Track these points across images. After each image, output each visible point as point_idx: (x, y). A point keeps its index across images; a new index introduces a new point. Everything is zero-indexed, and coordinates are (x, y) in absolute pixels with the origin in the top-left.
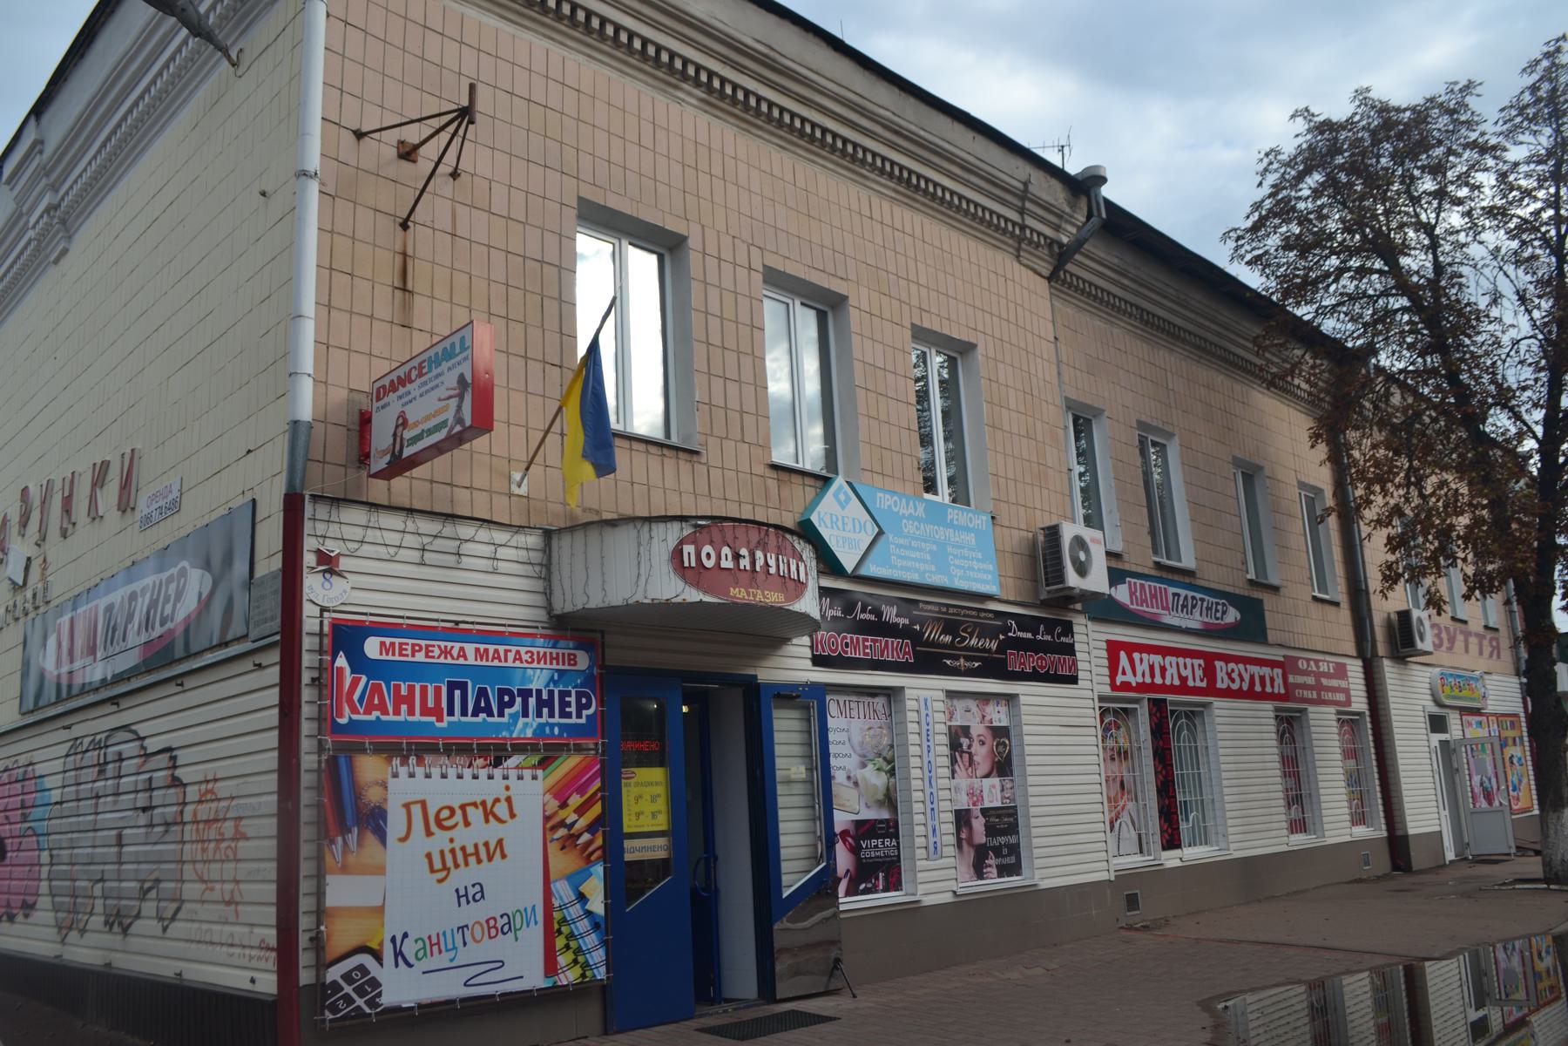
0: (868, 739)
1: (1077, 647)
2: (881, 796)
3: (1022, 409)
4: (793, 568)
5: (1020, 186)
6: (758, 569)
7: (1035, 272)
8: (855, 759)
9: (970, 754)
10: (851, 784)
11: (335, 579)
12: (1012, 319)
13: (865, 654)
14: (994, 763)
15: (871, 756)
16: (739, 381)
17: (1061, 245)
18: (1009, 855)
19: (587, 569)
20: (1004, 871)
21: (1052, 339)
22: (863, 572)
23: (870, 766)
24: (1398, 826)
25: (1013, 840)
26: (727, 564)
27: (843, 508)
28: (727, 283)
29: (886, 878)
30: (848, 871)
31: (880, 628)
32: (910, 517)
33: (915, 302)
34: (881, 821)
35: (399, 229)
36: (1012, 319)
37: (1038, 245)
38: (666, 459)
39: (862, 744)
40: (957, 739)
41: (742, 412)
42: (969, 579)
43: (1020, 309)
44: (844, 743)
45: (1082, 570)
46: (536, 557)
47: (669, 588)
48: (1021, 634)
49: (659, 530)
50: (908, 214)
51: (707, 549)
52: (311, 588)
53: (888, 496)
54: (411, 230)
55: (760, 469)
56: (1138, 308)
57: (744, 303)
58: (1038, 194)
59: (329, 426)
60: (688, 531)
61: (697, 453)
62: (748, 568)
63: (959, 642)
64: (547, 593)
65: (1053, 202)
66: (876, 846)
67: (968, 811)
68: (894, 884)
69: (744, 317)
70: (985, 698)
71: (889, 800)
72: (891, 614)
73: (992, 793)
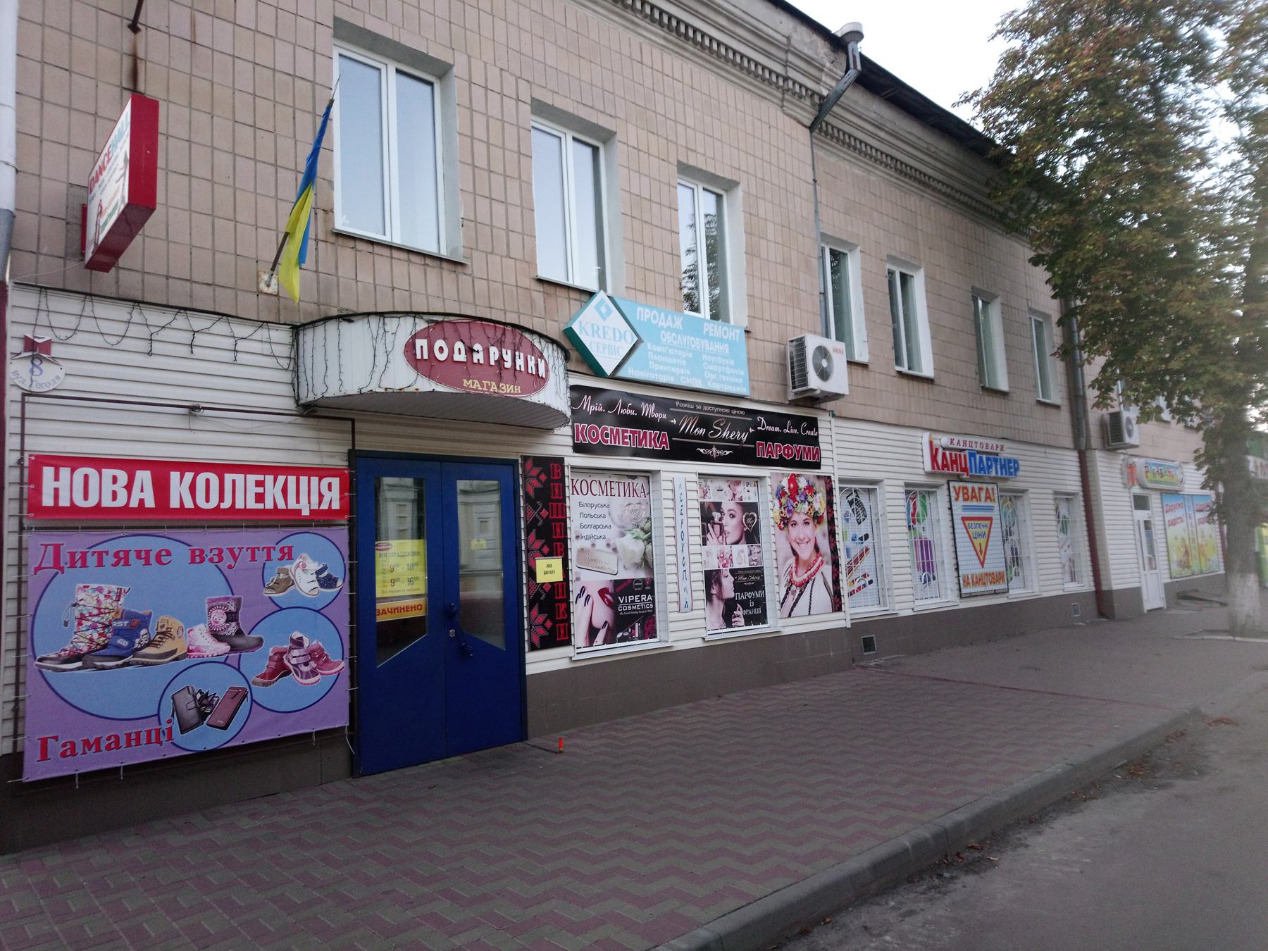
0: (627, 513)
1: (821, 439)
2: (638, 559)
3: (779, 240)
4: (531, 364)
5: (784, 40)
6: (492, 363)
7: (799, 122)
8: (615, 530)
9: (721, 525)
10: (610, 550)
11: (45, 366)
12: (774, 161)
13: (624, 443)
14: (742, 532)
15: (630, 527)
16: (505, 202)
17: (821, 97)
18: (755, 607)
19: (326, 361)
20: (749, 620)
21: (812, 182)
22: (621, 374)
23: (629, 535)
24: (1103, 582)
25: (759, 594)
26: (460, 357)
27: (604, 319)
28: (494, 111)
29: (642, 627)
30: (606, 622)
31: (640, 422)
32: (669, 328)
33: (682, 142)
34: (637, 581)
35: (128, 33)
36: (774, 161)
37: (800, 97)
38: (429, 269)
39: (621, 517)
40: (708, 514)
41: (508, 231)
42: (672, 374)
43: (781, 154)
44: (604, 517)
45: (824, 375)
46: (284, 351)
47: (402, 377)
48: (769, 428)
49: (391, 323)
50: (678, 62)
51: (440, 343)
52: (16, 373)
53: (647, 310)
54: (142, 34)
55: (526, 282)
56: (892, 158)
57: (511, 131)
58: (800, 48)
59: (44, 220)
60: (421, 325)
61: (462, 264)
62: (482, 362)
63: (711, 434)
64: (295, 384)
65: (815, 57)
66: (633, 601)
67: (718, 571)
68: (649, 631)
69: (511, 144)
70: (736, 480)
71: (647, 563)
72: (649, 410)
73: (741, 556)
